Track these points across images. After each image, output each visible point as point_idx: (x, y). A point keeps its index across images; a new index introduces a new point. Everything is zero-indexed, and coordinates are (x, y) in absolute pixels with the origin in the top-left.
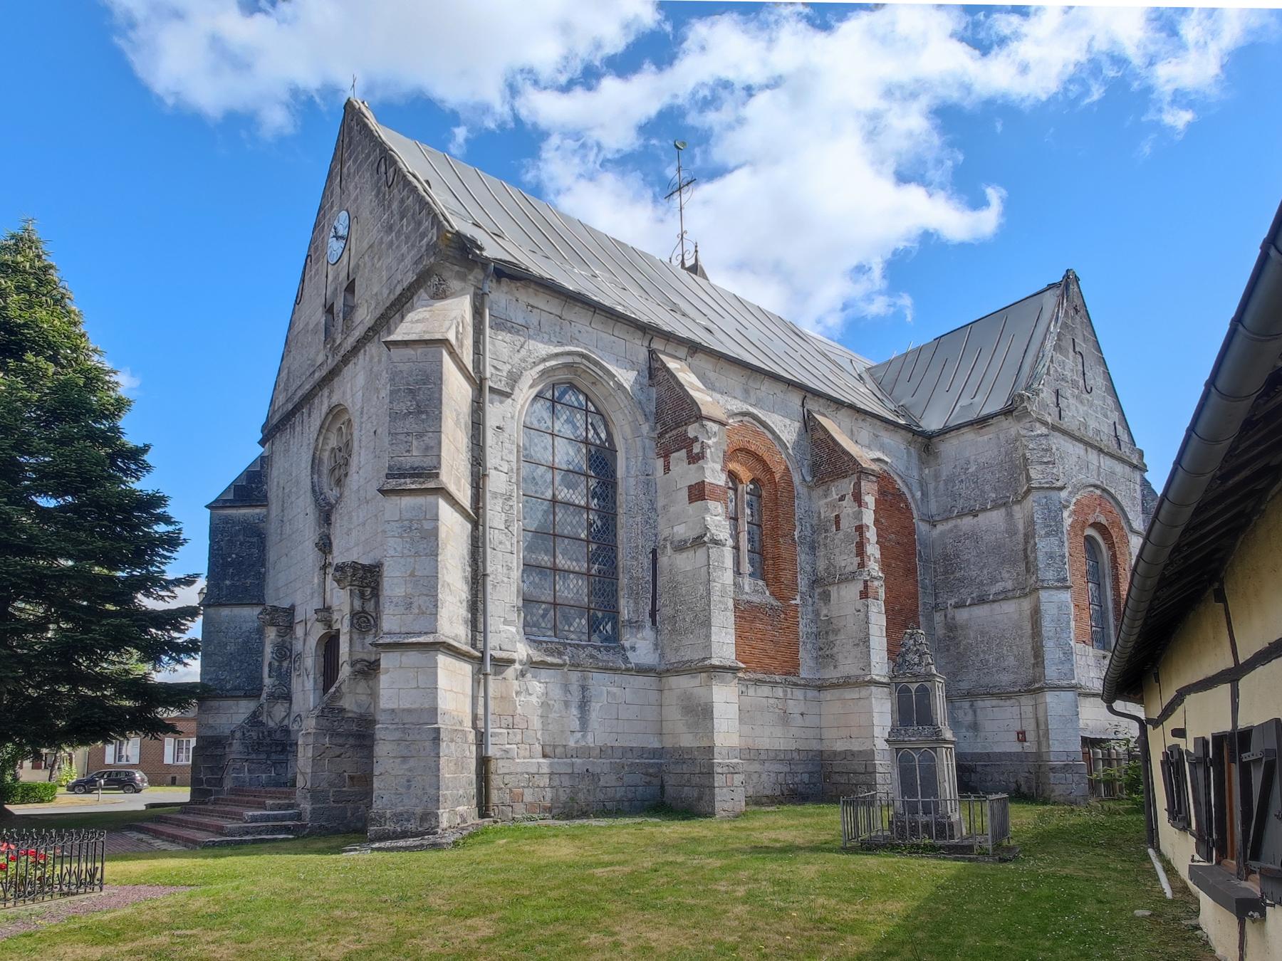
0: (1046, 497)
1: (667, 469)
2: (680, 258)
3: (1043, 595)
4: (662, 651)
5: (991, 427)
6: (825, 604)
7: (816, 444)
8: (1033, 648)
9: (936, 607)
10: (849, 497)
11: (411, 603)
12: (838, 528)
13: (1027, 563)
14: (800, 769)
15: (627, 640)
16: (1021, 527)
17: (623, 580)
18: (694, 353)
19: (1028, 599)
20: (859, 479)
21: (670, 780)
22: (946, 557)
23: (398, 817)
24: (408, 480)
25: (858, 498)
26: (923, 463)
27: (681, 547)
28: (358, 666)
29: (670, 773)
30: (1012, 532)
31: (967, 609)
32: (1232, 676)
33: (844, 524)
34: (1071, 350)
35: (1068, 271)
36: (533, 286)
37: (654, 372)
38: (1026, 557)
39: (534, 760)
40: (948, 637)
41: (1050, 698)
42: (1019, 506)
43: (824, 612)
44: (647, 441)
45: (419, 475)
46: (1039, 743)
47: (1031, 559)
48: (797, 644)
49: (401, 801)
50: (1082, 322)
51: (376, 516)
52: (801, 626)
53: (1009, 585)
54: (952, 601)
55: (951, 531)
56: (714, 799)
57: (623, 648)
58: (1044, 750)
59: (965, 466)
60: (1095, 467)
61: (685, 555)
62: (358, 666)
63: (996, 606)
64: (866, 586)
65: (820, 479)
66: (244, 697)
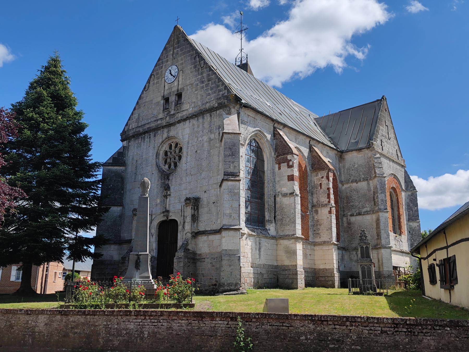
0: (381, 180)
1: (279, 168)
2: (240, 59)
3: (381, 214)
4: (277, 231)
5: (363, 152)
6: (316, 214)
7: (313, 157)
8: (377, 233)
9: (344, 215)
10: (325, 177)
11: (231, 215)
12: (321, 188)
13: (374, 202)
14: (310, 275)
15: (268, 227)
16: (372, 189)
17: (266, 206)
18: (285, 127)
19: (375, 215)
20: (328, 171)
21: (281, 277)
22: (347, 197)
23: (229, 285)
24: (230, 177)
25: (328, 178)
26: (340, 161)
27: (285, 195)
28: (193, 234)
29: (280, 274)
30: (369, 190)
31: (354, 217)
32: (447, 247)
33: (323, 187)
34: (385, 125)
35: (383, 96)
36: (250, 109)
37: (275, 135)
38: (374, 200)
39: (249, 268)
40: (348, 227)
41: (383, 251)
42: (371, 181)
43: (316, 217)
44: (273, 158)
45: (233, 175)
46: (379, 268)
47: (376, 200)
48: (308, 229)
49: (229, 280)
50: (387, 114)
51: (197, 181)
52: (309, 222)
53: (368, 209)
54: (349, 214)
55: (349, 188)
56: (297, 283)
57: (266, 229)
58: (381, 270)
59: (354, 165)
60: (392, 167)
61: (286, 198)
62: (193, 234)
63: (364, 216)
64: (331, 209)
65: (315, 170)
66: (114, 244)
